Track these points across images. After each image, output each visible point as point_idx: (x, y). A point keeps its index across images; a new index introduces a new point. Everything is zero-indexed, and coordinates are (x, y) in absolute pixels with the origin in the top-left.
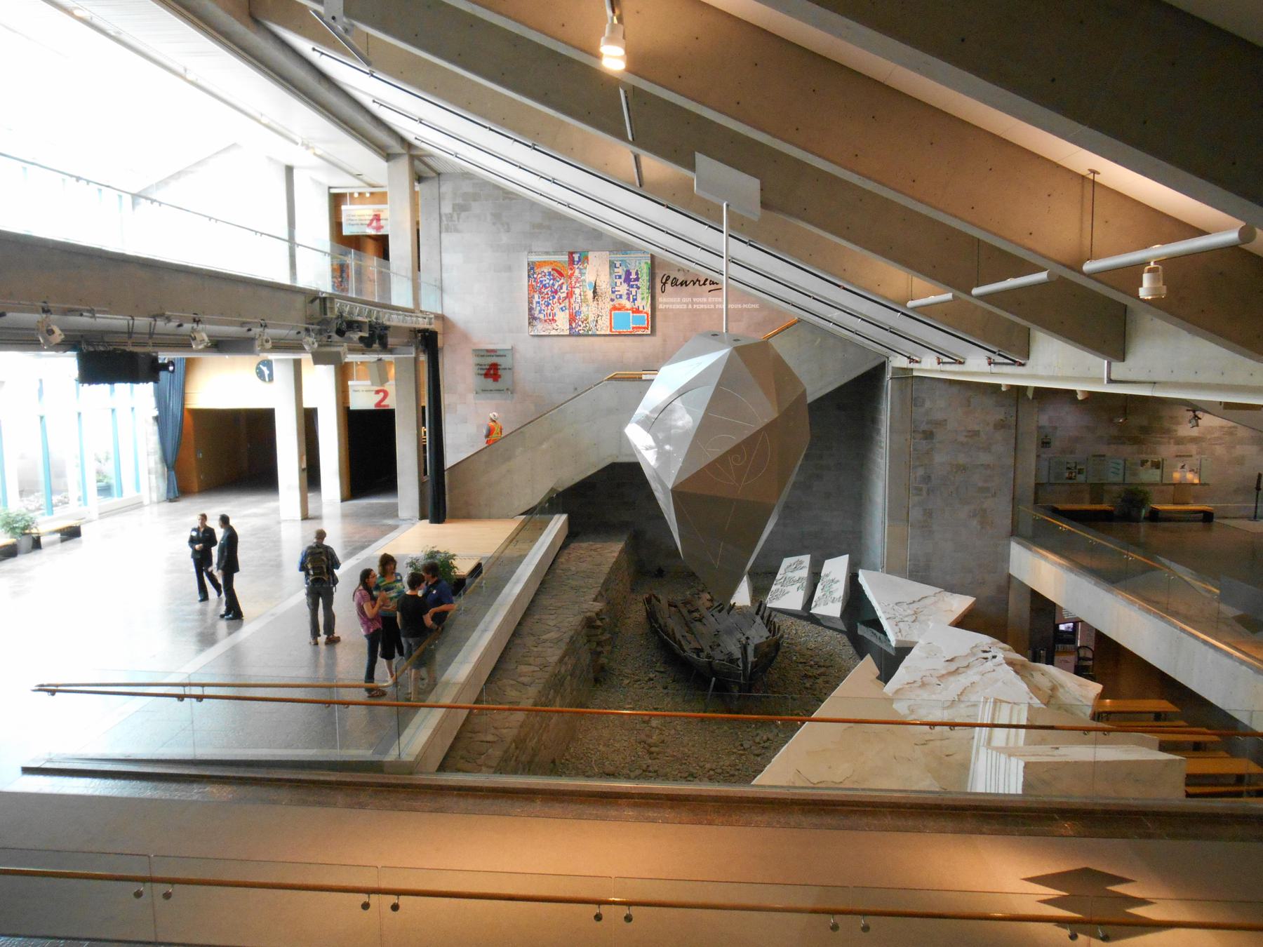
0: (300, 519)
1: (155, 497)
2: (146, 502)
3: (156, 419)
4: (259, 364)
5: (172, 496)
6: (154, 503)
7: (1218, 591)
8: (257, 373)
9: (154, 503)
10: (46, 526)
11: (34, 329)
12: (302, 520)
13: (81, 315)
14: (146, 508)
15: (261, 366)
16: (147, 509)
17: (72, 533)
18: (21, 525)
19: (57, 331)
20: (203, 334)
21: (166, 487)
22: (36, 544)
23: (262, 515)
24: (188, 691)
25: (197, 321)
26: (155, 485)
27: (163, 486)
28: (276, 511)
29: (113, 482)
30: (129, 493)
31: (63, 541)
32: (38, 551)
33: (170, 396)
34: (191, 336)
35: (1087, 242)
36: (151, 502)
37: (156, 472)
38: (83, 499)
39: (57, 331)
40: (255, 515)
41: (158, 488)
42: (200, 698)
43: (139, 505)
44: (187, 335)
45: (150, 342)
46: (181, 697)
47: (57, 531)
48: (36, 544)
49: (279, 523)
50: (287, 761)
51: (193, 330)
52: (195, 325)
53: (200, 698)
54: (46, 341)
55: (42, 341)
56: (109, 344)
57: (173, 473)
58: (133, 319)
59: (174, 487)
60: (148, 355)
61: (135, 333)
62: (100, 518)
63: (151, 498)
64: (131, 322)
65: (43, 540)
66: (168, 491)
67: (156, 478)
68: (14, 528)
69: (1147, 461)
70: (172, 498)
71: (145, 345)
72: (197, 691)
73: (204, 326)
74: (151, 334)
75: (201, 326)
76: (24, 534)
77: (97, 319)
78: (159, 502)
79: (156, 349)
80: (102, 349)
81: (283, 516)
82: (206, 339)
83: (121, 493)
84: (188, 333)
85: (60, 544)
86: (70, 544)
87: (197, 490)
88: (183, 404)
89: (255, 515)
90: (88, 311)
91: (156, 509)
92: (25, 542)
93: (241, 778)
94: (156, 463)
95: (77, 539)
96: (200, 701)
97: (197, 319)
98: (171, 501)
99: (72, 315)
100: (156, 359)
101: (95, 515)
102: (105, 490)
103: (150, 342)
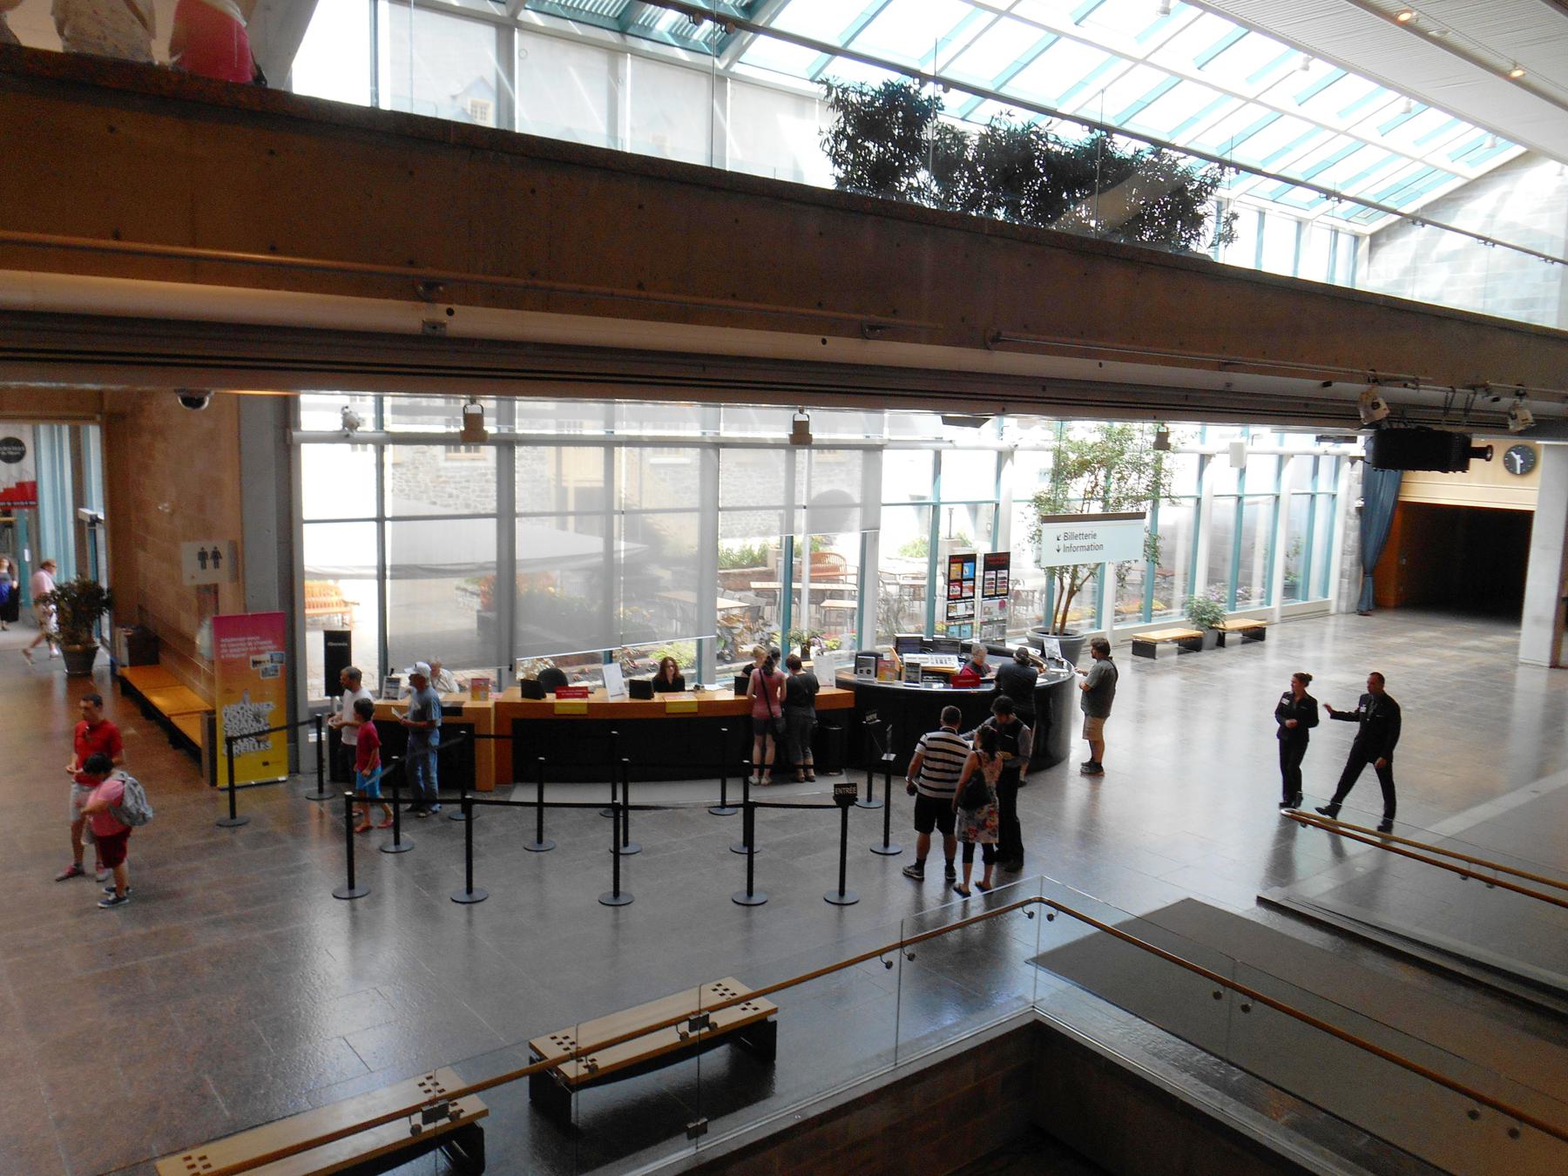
0: (1548, 665)
1: (1343, 605)
2: (1333, 611)
3: (1359, 510)
4: (1510, 450)
5: (1364, 608)
6: (1342, 613)
7: (1380, 759)
8: (1505, 462)
9: (1342, 613)
10: (1234, 623)
11: (1354, 402)
12: (1551, 667)
13: (1405, 386)
14: (1332, 618)
15: (1513, 453)
16: (1332, 620)
17: (1255, 635)
18: (1210, 617)
19: (1383, 405)
20: (1527, 412)
21: (1359, 594)
22: (1221, 642)
23: (1489, 651)
24: (1474, 868)
25: (1520, 395)
26: (1346, 591)
27: (1356, 593)
28: (1515, 647)
29: (1300, 581)
30: (1315, 596)
31: (1244, 642)
32: (1222, 649)
33: (1381, 485)
34: (1510, 414)
35: (1326, 226)
36: (1339, 612)
37: (1350, 576)
38: (1267, 597)
39: (1383, 405)
40: (1476, 649)
41: (1349, 595)
42: (1491, 883)
43: (1322, 613)
44: (1505, 413)
45: (1465, 421)
46: (1466, 874)
47: (1240, 630)
48: (1221, 642)
49: (1515, 665)
50: (1533, 981)
51: (1515, 406)
52: (1517, 400)
53: (1491, 883)
54: (1368, 415)
55: (1362, 416)
56: (1412, 421)
57: (1370, 579)
58: (1454, 391)
59: (1369, 599)
60: (1461, 435)
61: (1473, 411)
62: (1283, 622)
63: (1338, 606)
64: (1450, 394)
65: (1228, 637)
66: (1361, 600)
67: (1349, 583)
68: (1202, 620)
69: (1294, 555)
70: (1364, 610)
71: (1457, 423)
72: (1488, 873)
73: (1528, 401)
74: (1467, 410)
75: (1525, 401)
76: (1212, 628)
77: (1421, 391)
78: (1347, 613)
79: (1470, 429)
80: (1402, 426)
81: (1523, 655)
82: (1531, 419)
83: (1306, 598)
84: (1507, 410)
85: (1240, 646)
86: (1252, 647)
87: (1393, 604)
88: (1397, 496)
89: (1476, 649)
90: (1413, 381)
91: (1343, 620)
92: (1211, 638)
93: (1506, 993)
94: (1352, 565)
95: (1260, 642)
96: (1464, 879)
97: (1521, 392)
98: (1362, 614)
99: (1389, 386)
100: (1469, 442)
101: (1277, 618)
102: (1290, 590)
103: (1465, 421)
